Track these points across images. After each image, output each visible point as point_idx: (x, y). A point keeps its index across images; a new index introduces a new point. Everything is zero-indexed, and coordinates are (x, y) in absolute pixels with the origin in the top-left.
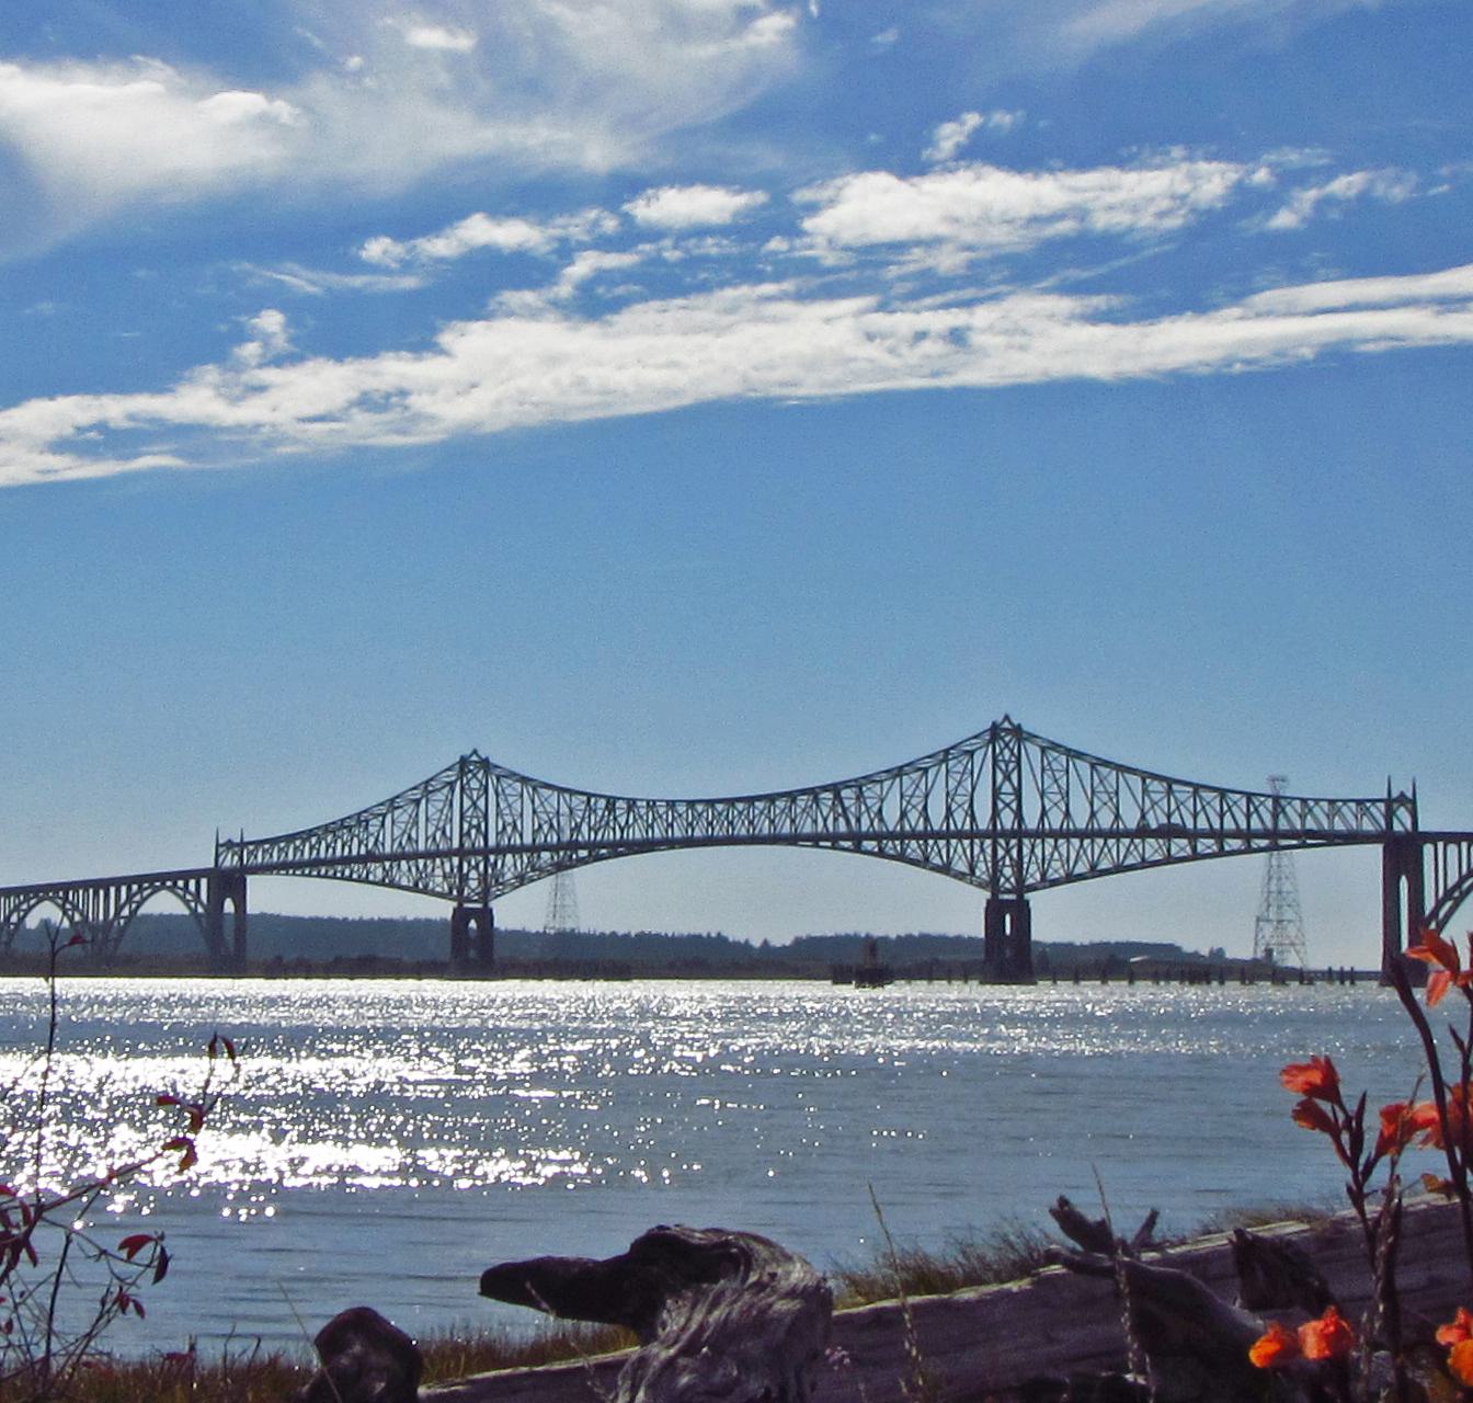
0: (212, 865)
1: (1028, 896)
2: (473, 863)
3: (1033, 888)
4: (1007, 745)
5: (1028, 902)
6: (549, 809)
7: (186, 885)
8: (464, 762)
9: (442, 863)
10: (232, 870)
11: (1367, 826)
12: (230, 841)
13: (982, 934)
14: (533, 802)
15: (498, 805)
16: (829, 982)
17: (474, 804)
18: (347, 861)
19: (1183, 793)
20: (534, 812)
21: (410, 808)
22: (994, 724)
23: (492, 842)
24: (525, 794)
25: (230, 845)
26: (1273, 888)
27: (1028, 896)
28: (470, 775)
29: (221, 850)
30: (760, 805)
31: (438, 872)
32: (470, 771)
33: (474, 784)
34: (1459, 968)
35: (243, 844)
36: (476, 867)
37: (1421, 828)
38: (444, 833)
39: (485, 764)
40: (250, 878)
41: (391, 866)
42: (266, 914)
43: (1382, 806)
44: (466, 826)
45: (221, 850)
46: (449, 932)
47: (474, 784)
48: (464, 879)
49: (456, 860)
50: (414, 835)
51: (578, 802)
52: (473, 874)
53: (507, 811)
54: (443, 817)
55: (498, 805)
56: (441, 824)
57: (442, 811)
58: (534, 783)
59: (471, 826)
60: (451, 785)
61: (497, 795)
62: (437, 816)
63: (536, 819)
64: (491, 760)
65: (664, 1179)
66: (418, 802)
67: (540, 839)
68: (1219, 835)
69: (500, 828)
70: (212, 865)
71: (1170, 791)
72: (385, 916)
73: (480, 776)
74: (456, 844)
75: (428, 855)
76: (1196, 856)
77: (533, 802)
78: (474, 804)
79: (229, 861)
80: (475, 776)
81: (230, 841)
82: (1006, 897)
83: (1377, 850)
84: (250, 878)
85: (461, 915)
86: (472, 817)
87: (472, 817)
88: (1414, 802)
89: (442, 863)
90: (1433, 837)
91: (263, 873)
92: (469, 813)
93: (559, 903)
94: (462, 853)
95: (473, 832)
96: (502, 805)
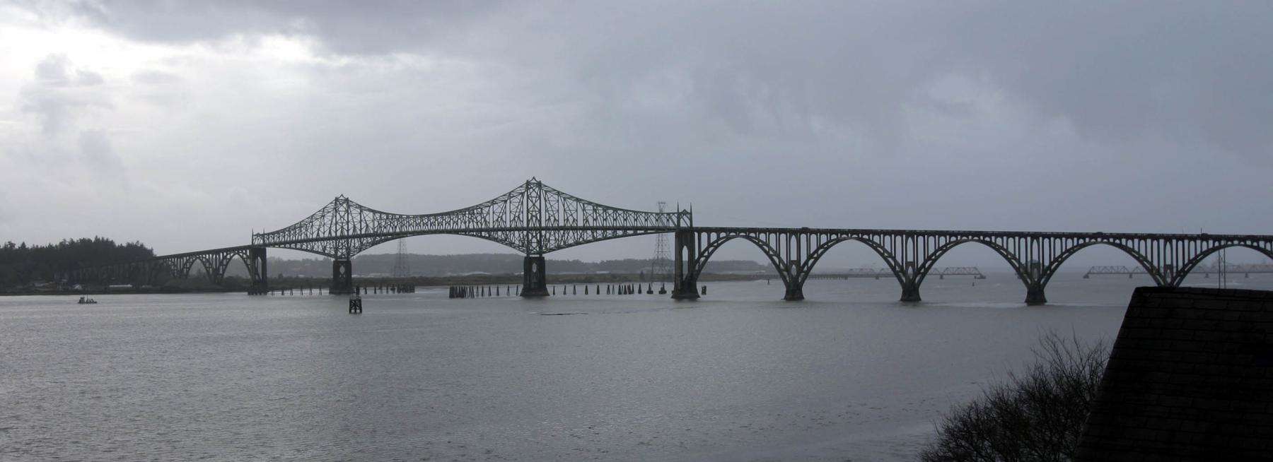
0: (251, 244)
1: (543, 255)
2: (534, 234)
3: (545, 253)
4: (534, 190)
5: (544, 258)
6: (554, 209)
7: (246, 252)
8: (528, 183)
9: (555, 234)
10: (259, 245)
11: (671, 225)
12: (685, 210)
13: (332, 277)
14: (564, 205)
15: (546, 206)
16: (246, 293)
17: (534, 205)
18: (296, 242)
19: (600, 210)
20: (565, 210)
21: (502, 204)
22: (527, 181)
23: (543, 225)
24: (560, 200)
25: (258, 235)
26: (660, 250)
27: (543, 255)
28: (531, 190)
29: (254, 237)
30: (610, 211)
31: (552, 238)
32: (531, 188)
33: (534, 194)
34: (667, 281)
35: (263, 235)
36: (536, 237)
37: (694, 225)
38: (502, 219)
39: (539, 185)
40: (267, 249)
41: (564, 233)
42: (580, 262)
43: (676, 215)
44: (530, 215)
45: (254, 237)
46: (353, 271)
47: (534, 194)
48: (530, 242)
49: (525, 232)
50: (487, 219)
51: (384, 217)
52: (534, 240)
53: (550, 209)
54: (518, 211)
55: (546, 206)
56: (517, 214)
57: (517, 207)
58: (564, 196)
59: (532, 216)
60: (522, 194)
61: (546, 201)
62: (515, 210)
63: (547, 214)
64: (349, 199)
65: (1063, 415)
66: (506, 201)
67: (531, 225)
68: (615, 229)
69: (547, 218)
70: (251, 244)
71: (595, 210)
72: (609, 259)
73: (536, 190)
74: (525, 225)
75: (547, 229)
76: (606, 238)
77: (564, 205)
78: (534, 205)
79: (259, 241)
80: (534, 190)
81: (685, 210)
82: (533, 256)
83: (672, 236)
84: (267, 249)
85: (528, 262)
86: (533, 211)
87: (533, 211)
88: (691, 214)
89: (555, 234)
90: (700, 230)
91: (717, 228)
92: (531, 209)
93: (660, 250)
94: (528, 229)
95: (534, 219)
96: (548, 206)
